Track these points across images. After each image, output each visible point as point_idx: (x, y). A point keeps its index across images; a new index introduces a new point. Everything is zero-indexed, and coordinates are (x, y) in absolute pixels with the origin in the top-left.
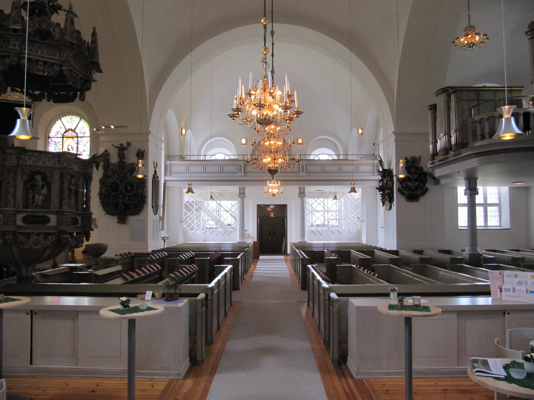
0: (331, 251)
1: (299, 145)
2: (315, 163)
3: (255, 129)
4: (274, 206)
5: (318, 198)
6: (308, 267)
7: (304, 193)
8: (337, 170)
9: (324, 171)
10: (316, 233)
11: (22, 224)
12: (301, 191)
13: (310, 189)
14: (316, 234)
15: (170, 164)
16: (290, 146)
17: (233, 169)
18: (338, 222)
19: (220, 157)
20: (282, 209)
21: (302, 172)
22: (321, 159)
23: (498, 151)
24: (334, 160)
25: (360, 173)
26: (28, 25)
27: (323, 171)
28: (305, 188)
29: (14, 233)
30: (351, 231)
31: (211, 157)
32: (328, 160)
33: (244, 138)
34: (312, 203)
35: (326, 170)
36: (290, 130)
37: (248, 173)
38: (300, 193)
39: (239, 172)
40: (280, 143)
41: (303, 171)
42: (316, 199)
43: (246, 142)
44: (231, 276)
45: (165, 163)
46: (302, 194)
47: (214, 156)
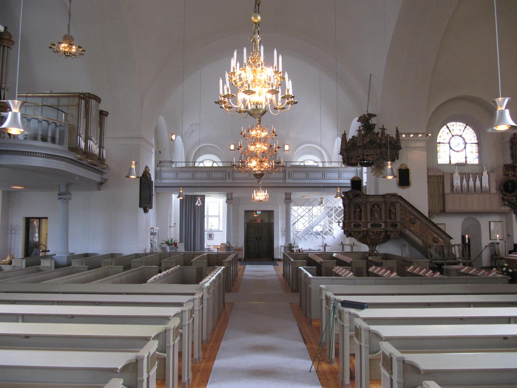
0: (315, 254)
1: (231, 151)
2: (319, 169)
3: (242, 134)
4: (261, 212)
5: (301, 206)
6: (300, 269)
7: (290, 199)
8: (206, 177)
9: (251, 178)
10: (301, 238)
11: (382, 223)
12: (288, 197)
13: (296, 195)
14: (301, 239)
15: (160, 171)
16: (275, 151)
17: (221, 175)
18: (322, 227)
19: (208, 164)
20: (270, 214)
21: (288, 179)
22: (206, 166)
23: (51, 156)
24: (219, 167)
25: (235, 179)
26: (22, 22)
27: (250, 178)
28: (291, 195)
29: (367, 231)
30: (335, 236)
31: (199, 164)
32: (212, 167)
33: (232, 144)
34: (296, 211)
35: (235, 176)
36: (275, 135)
37: (164, 179)
38: (286, 199)
39: (227, 178)
40: (266, 148)
41: (229, 178)
42: (307, 207)
43: (234, 148)
44: (224, 277)
45: (156, 169)
46: (288, 200)
47: (202, 163)
